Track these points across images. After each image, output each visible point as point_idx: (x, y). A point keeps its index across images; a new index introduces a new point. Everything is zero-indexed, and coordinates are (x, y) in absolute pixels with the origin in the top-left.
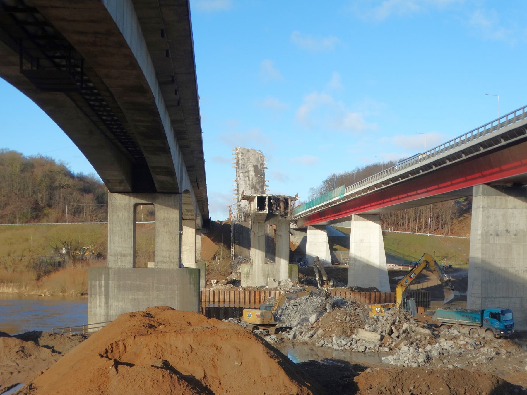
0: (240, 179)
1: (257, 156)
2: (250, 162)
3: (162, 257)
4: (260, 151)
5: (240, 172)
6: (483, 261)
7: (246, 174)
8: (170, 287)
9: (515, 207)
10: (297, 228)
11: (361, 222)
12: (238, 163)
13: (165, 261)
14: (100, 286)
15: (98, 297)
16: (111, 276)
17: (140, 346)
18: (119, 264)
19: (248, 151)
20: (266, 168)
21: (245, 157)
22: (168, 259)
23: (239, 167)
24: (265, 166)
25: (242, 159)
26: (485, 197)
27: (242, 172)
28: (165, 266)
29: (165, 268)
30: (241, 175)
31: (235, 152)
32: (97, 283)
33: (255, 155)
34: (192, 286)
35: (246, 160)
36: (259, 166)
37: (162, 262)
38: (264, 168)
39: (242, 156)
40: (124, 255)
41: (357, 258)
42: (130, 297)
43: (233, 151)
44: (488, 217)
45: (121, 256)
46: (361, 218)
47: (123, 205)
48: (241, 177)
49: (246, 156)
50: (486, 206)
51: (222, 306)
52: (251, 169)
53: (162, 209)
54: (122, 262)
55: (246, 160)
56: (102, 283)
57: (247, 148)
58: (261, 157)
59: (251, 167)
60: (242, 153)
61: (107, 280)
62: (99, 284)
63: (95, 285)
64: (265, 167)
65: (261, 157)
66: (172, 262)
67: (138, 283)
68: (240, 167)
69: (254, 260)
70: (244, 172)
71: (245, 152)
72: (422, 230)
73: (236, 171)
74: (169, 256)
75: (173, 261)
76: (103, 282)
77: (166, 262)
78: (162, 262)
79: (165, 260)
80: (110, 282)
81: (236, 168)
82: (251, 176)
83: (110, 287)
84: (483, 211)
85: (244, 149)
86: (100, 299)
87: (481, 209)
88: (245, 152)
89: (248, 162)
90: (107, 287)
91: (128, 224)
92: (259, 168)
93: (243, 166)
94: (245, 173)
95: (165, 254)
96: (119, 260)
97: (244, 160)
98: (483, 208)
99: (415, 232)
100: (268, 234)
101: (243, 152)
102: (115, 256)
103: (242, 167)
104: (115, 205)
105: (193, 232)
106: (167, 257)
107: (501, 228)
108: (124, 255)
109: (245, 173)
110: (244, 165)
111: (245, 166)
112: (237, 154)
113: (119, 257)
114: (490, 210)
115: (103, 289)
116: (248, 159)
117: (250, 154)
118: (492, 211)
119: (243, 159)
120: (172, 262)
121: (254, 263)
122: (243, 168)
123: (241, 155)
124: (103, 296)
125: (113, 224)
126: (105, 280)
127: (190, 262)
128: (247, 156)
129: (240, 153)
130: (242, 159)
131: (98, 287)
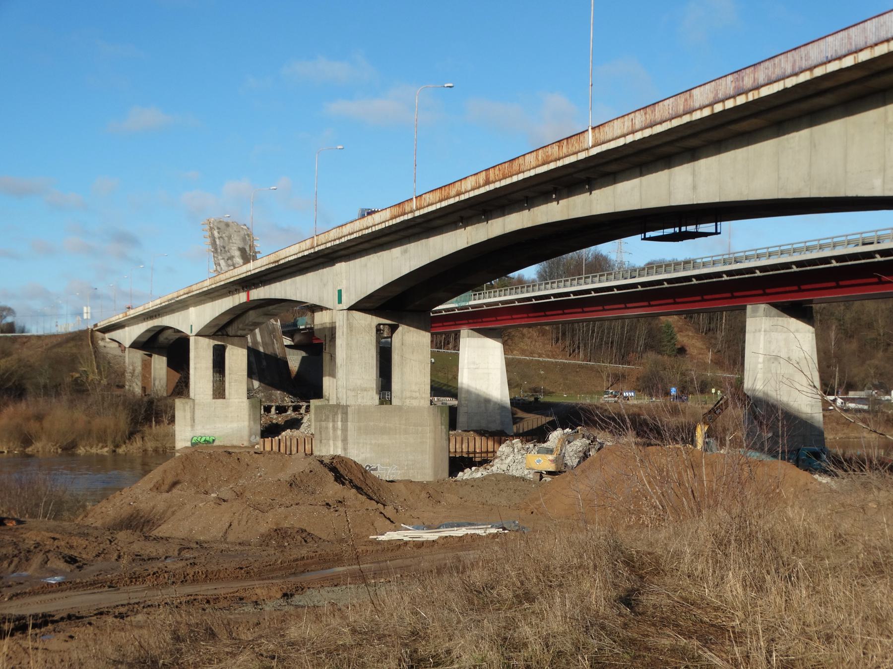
0: (221, 268)
1: (242, 233)
2: (233, 243)
3: (411, 391)
4: (245, 225)
5: (220, 257)
6: (765, 394)
7: (230, 262)
8: (420, 429)
9: (797, 331)
10: (293, 344)
11: (476, 339)
12: (214, 243)
13: (414, 396)
14: (335, 429)
15: (331, 442)
16: (350, 417)
17: (179, 520)
18: (359, 400)
19: (227, 225)
20: (259, 252)
21: (224, 235)
22: (417, 394)
23: (216, 249)
24: (257, 250)
25: (219, 238)
26: (768, 318)
27: (223, 259)
28: (415, 403)
29: (415, 404)
30: (222, 263)
31: (207, 227)
32: (331, 425)
33: (239, 232)
34: (443, 427)
35: (226, 239)
36: (248, 249)
37: (411, 398)
38: (256, 253)
39: (219, 233)
40: (365, 390)
41: (471, 389)
42: (373, 442)
43: (203, 224)
44: (770, 342)
45: (362, 390)
46: (476, 334)
47: (363, 325)
48: (222, 266)
49: (224, 233)
50: (768, 329)
51: (466, 456)
52: (237, 253)
53: (410, 331)
54: (363, 398)
55: (226, 239)
56: (337, 425)
57: (225, 220)
58: (248, 235)
59: (235, 250)
60: (218, 228)
61: (345, 420)
62: (334, 426)
63: (327, 428)
64: (256, 250)
65: (248, 235)
66: (422, 398)
67: (382, 424)
68: (219, 251)
69: (331, 395)
70: (226, 258)
71: (222, 226)
72: (450, 346)
73: (214, 256)
74: (419, 390)
75: (423, 396)
76: (339, 424)
77: (416, 398)
78: (411, 398)
79: (414, 395)
80: (349, 423)
81: (213, 251)
82: (238, 264)
83: (349, 429)
84: (765, 335)
85: (220, 222)
86: (334, 444)
87: (762, 333)
88: (222, 226)
89: (229, 242)
90: (345, 430)
91: (370, 350)
92: (248, 252)
93: (222, 249)
94: (228, 260)
95: (414, 388)
96: (359, 396)
97: (224, 239)
98: (765, 331)
99: (441, 348)
100: (276, 354)
101: (219, 226)
102: (354, 390)
103: (221, 250)
104: (354, 326)
105: (244, 355)
106: (416, 392)
107: (783, 354)
108: (365, 390)
109: (228, 260)
110: (224, 248)
111: (227, 249)
112: (211, 229)
113: (359, 392)
114: (772, 333)
115: (339, 432)
116: (230, 237)
117: (230, 229)
118: (774, 335)
119: (221, 237)
120: (422, 398)
121: (331, 398)
122: (223, 252)
123: (217, 230)
124: (340, 442)
125: (351, 349)
126: (342, 421)
127: (240, 398)
128: (227, 234)
129: (216, 228)
130: (219, 238)
131: (331, 431)
